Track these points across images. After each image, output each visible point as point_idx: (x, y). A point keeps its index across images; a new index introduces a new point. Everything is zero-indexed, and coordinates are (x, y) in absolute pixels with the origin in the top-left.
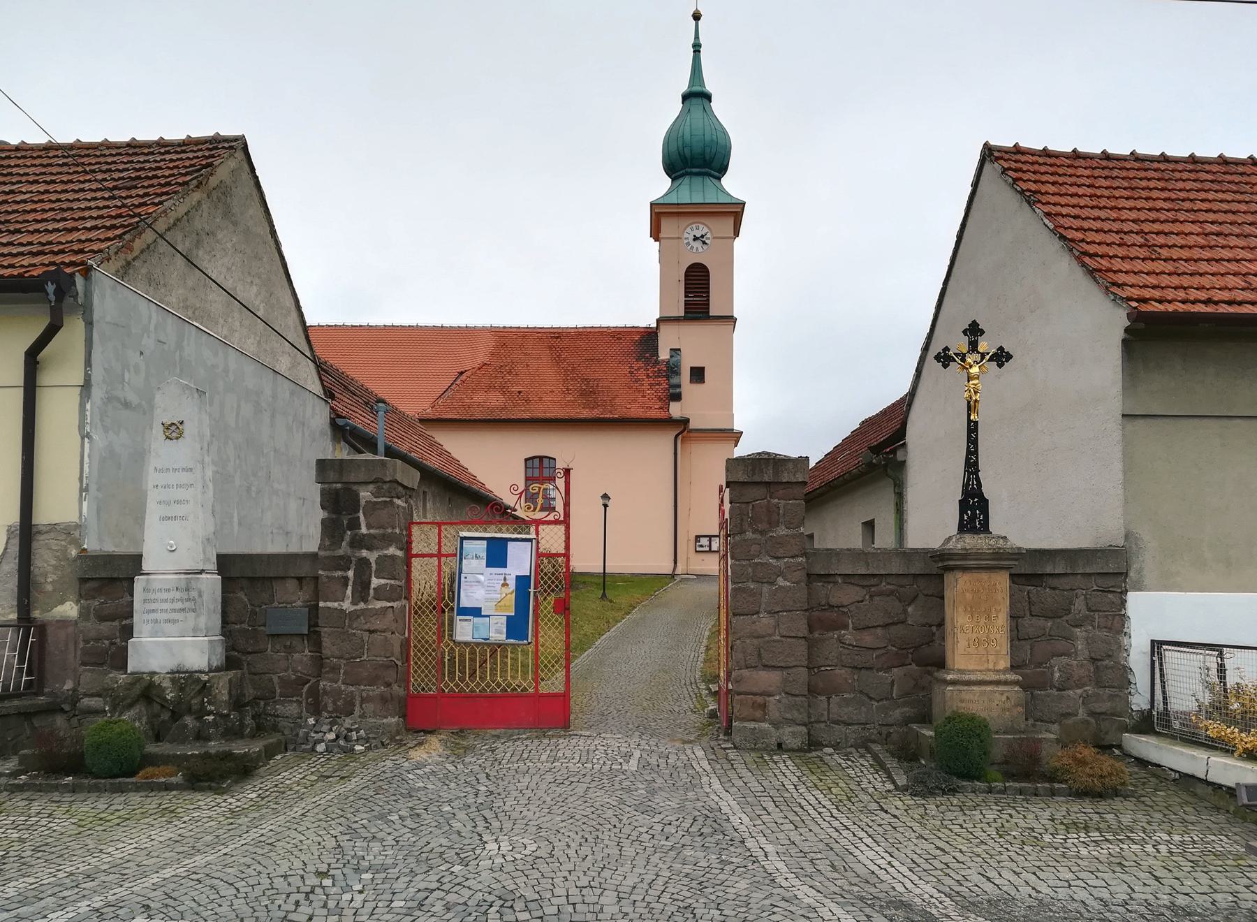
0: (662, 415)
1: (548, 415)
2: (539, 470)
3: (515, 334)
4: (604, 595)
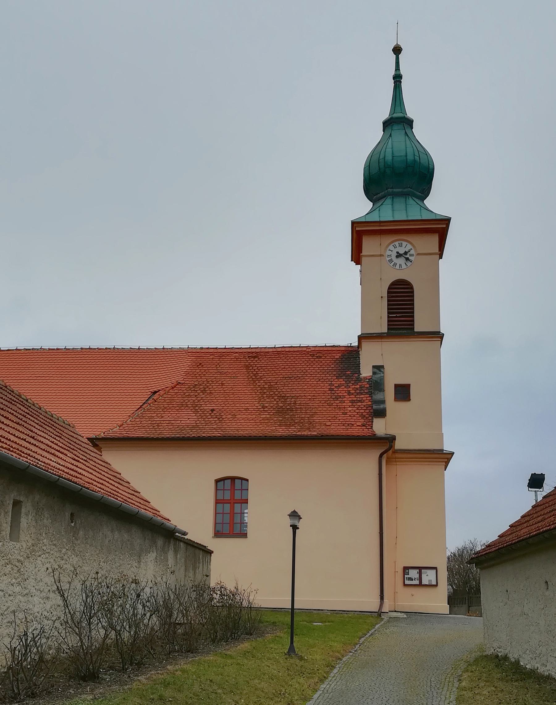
0: (365, 432)
1: (241, 433)
2: (231, 495)
3: (212, 354)
4: (292, 649)
